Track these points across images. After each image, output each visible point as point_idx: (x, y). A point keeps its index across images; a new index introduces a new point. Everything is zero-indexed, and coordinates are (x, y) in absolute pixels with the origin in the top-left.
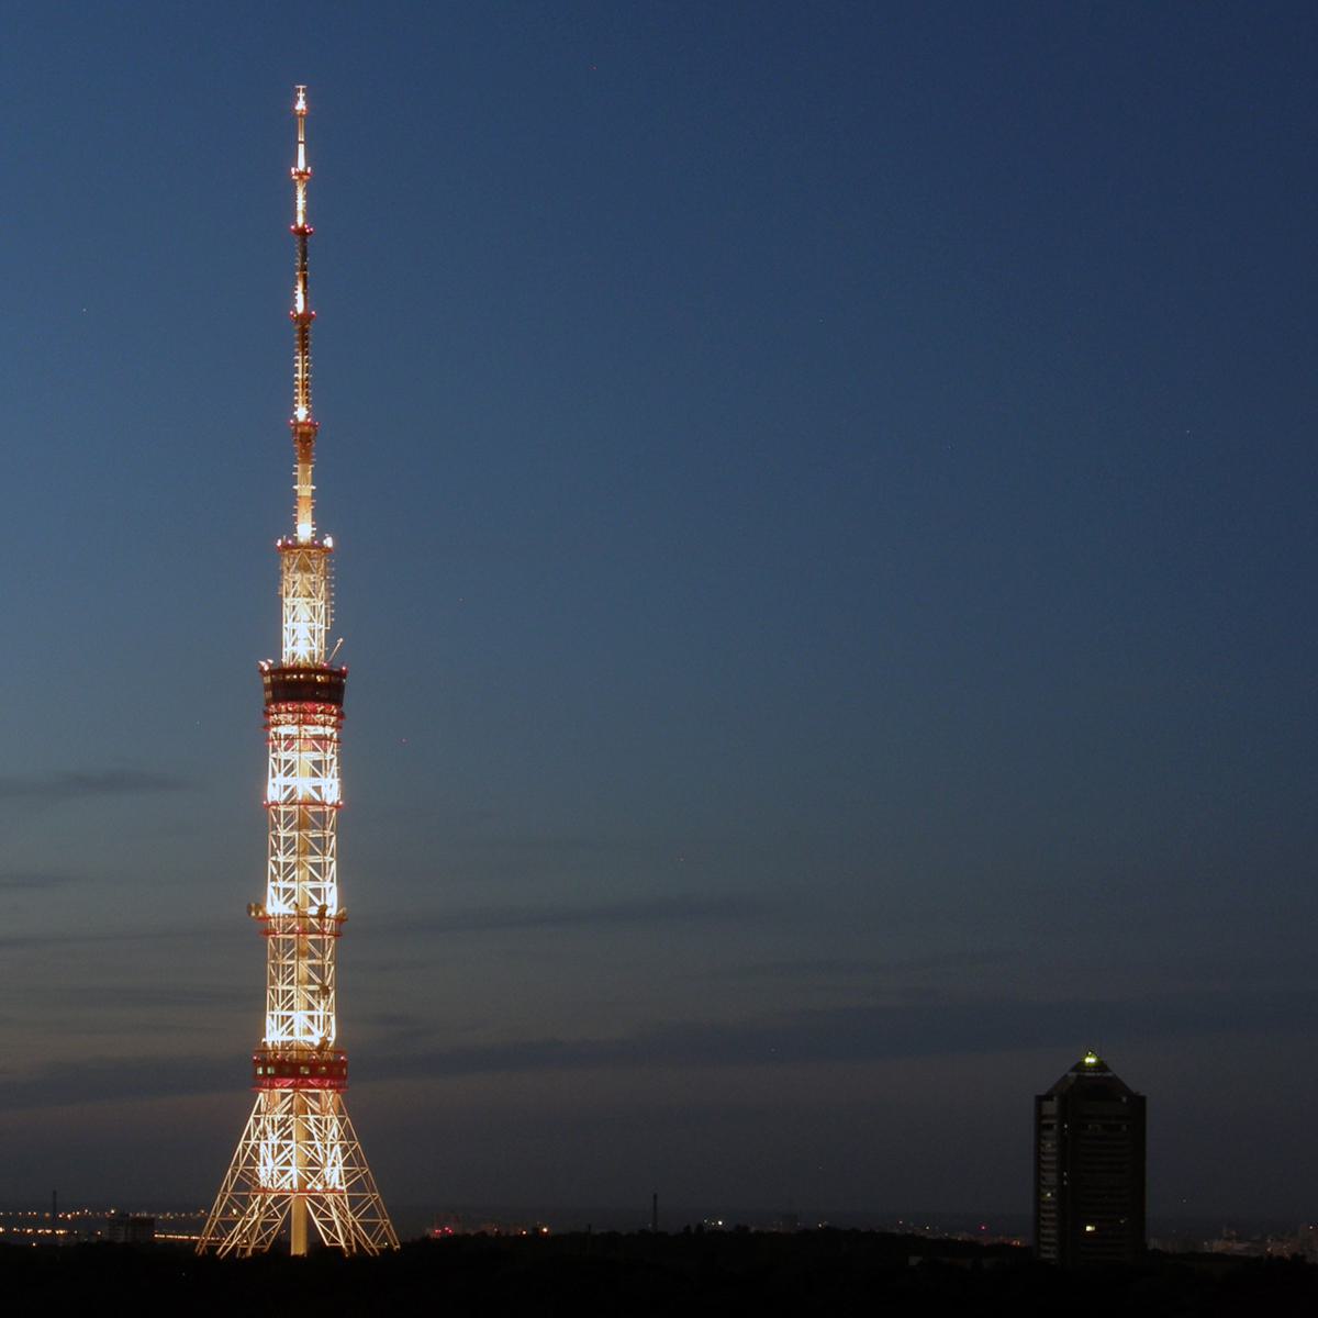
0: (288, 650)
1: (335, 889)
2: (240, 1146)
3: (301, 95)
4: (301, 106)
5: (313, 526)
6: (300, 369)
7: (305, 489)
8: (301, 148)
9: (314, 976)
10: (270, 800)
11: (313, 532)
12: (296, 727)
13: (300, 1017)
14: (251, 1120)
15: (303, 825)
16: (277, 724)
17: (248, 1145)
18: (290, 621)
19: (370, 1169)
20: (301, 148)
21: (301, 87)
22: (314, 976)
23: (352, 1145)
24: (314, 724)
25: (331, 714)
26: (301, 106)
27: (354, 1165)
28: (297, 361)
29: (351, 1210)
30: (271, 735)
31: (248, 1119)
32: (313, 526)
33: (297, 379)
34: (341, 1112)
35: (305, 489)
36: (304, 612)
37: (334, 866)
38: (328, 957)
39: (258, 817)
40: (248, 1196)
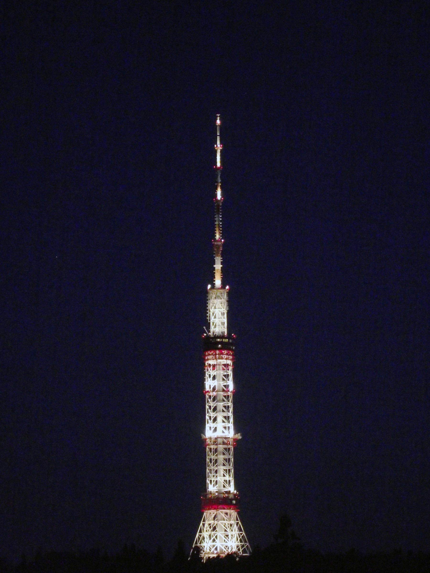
0: (212, 329)
1: (233, 481)
3: (218, 118)
4: (218, 122)
7: (218, 266)
8: (218, 138)
11: (221, 260)
14: (201, 524)
15: (224, 443)
16: (208, 360)
17: (200, 535)
19: (250, 544)
20: (218, 138)
21: (218, 115)
23: (241, 534)
24: (222, 358)
25: (230, 355)
26: (218, 122)
28: (216, 218)
30: (206, 364)
31: (200, 524)
32: (221, 260)
33: (216, 225)
35: (218, 266)
36: (218, 305)
37: (233, 459)
38: (231, 465)
40: (243, 554)
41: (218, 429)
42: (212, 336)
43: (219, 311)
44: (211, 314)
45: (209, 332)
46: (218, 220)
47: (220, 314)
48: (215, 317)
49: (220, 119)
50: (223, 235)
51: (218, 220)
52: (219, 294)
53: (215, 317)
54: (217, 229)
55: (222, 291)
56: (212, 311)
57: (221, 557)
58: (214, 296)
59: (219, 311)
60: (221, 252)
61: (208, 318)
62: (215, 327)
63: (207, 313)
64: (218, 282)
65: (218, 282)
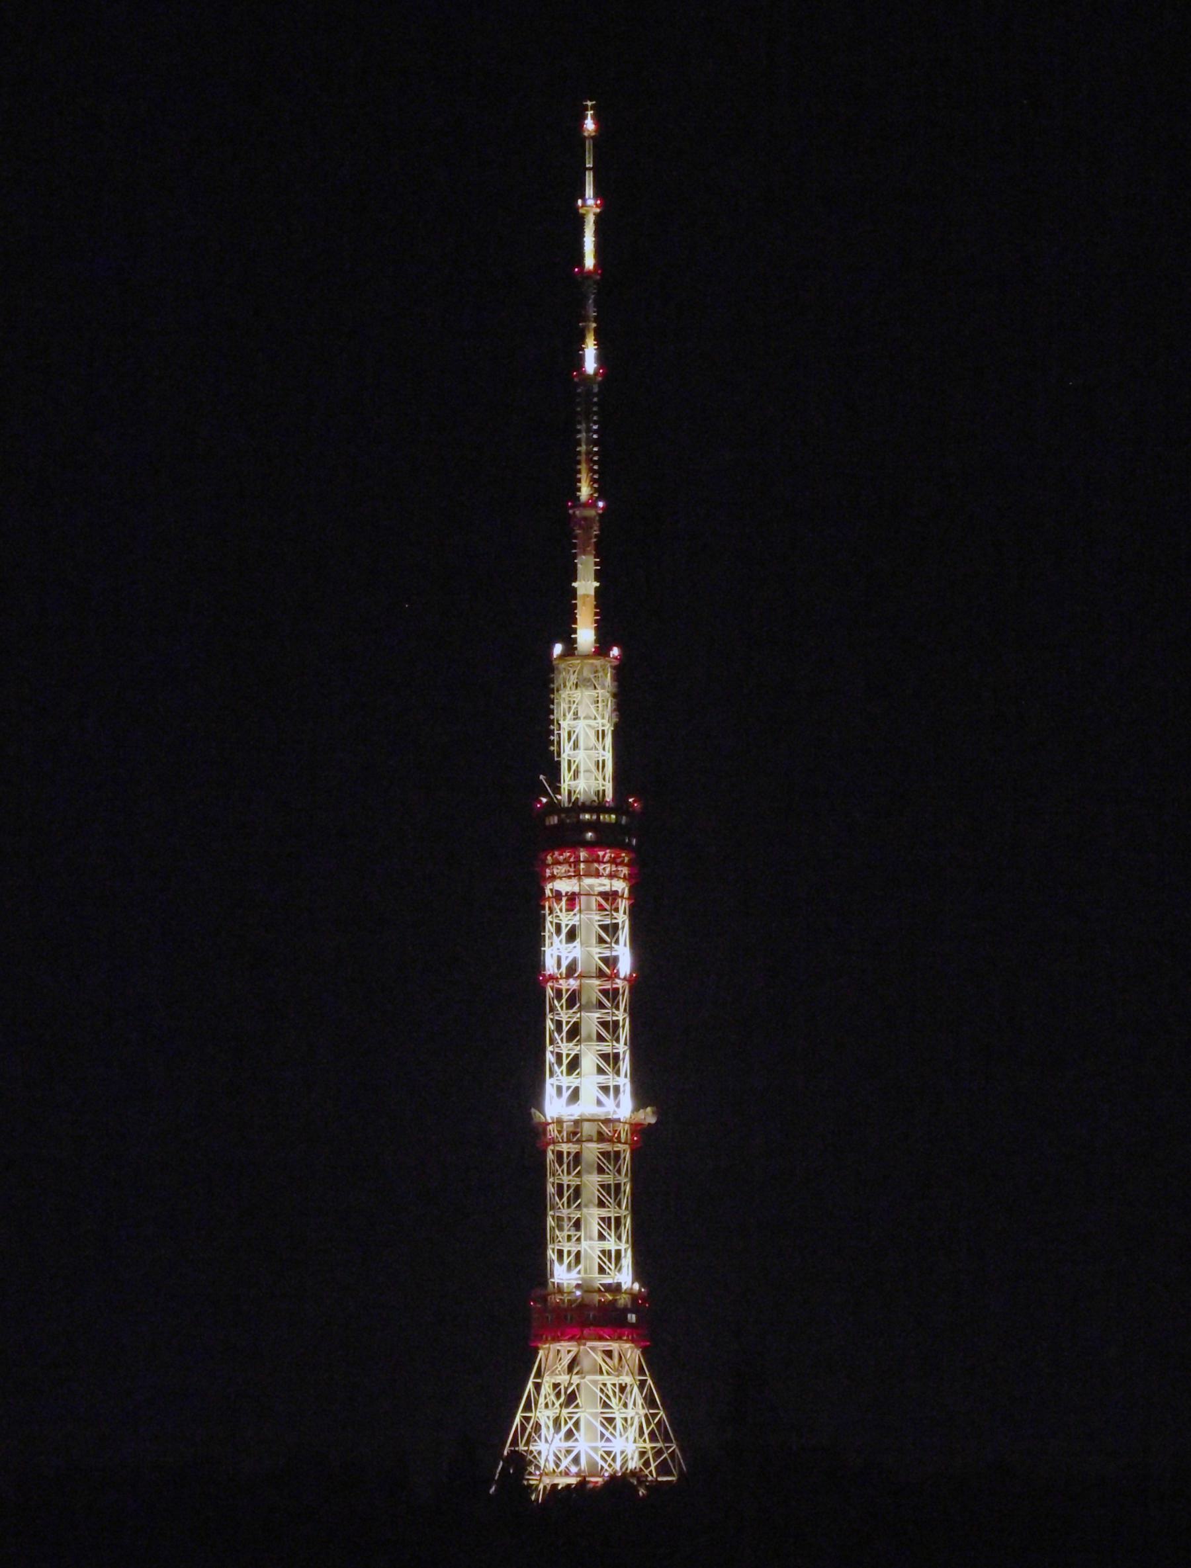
2: (517, 1420)
4: (590, 125)
5: (596, 564)
6: (584, 440)
7: (586, 586)
8: (589, 178)
9: (604, 1033)
10: (548, 973)
12: (574, 881)
13: (589, 1080)
17: (527, 1419)
18: (570, 716)
20: (589, 178)
21: (589, 103)
22: (604, 1033)
24: (598, 875)
25: (622, 863)
26: (590, 125)
27: (657, 1441)
28: (579, 432)
29: (655, 1461)
33: (579, 452)
34: (641, 1371)
35: (586, 586)
39: (527, 1141)
45: (557, 790)
46: (587, 439)
50: (602, 490)
51: (587, 439)
52: (587, 673)
54: (583, 467)
55: (598, 662)
58: (573, 678)
59: (589, 726)
62: (576, 775)
64: (586, 636)
65: (586, 636)
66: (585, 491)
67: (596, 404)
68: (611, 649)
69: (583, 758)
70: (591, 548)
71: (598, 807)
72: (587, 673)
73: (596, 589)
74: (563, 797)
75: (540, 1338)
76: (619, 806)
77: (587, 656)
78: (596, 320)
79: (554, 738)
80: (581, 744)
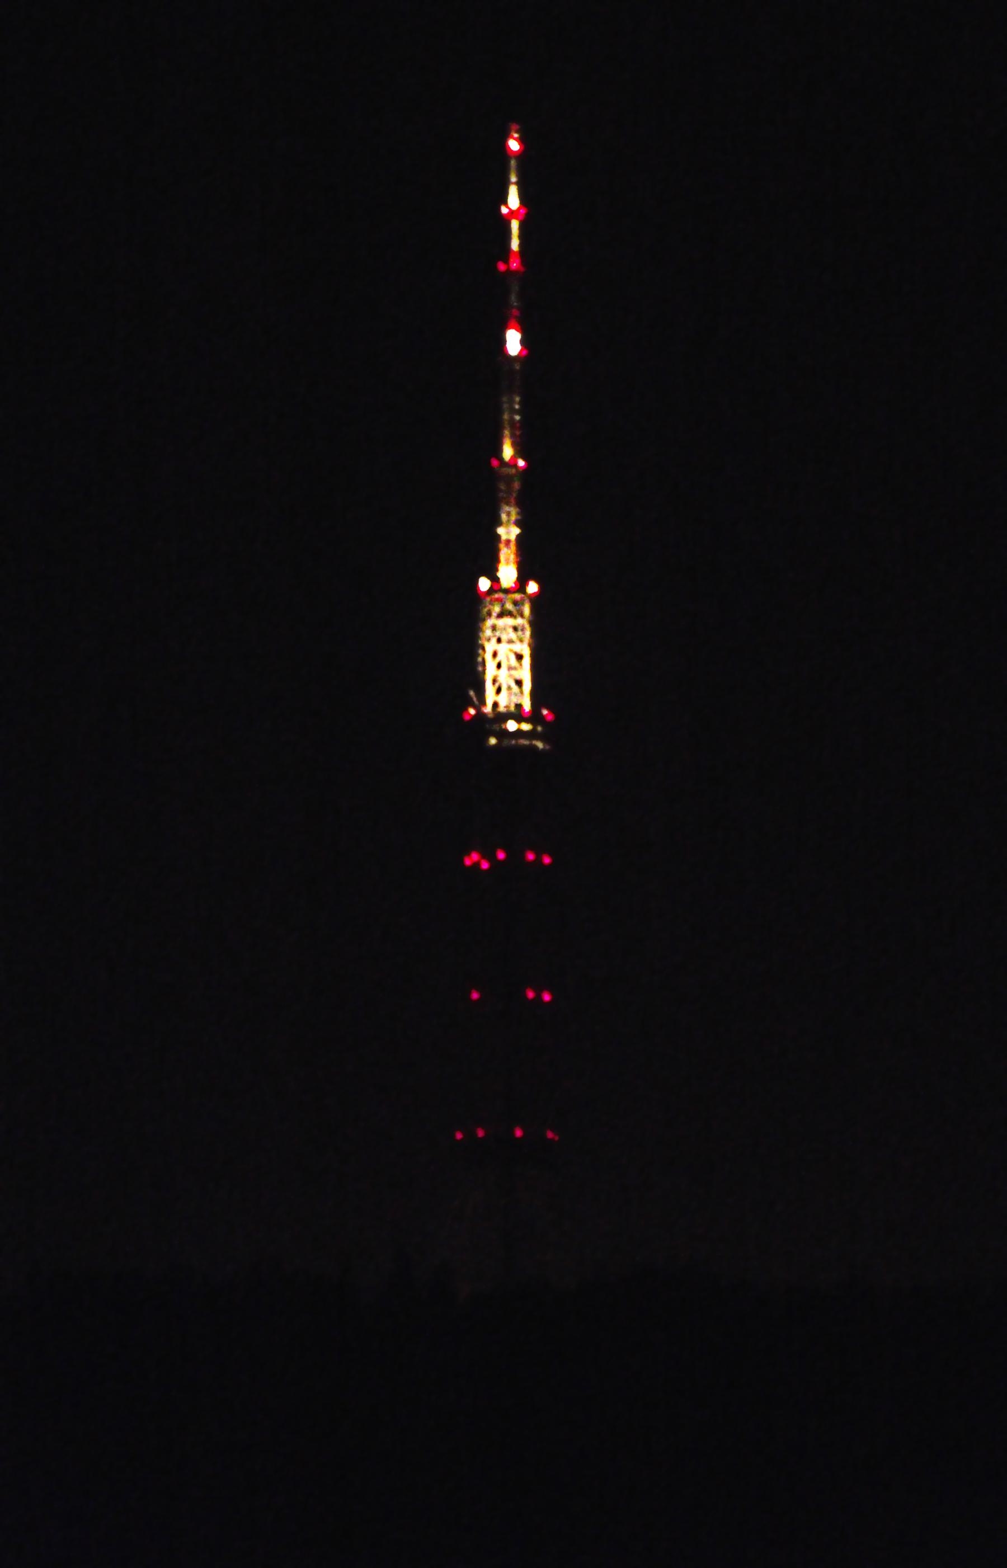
7: (509, 532)
18: (494, 640)
35: (509, 532)
41: (503, 665)
42: (491, 716)
43: (511, 650)
44: (488, 656)
45: (483, 702)
46: (513, 410)
47: (513, 657)
48: (499, 666)
49: (514, 445)
50: (520, 450)
51: (513, 410)
52: (509, 606)
53: (499, 691)
54: (507, 432)
55: (517, 596)
56: (490, 647)
57: (519, 517)
58: (497, 609)
59: (511, 650)
60: (515, 495)
61: (480, 669)
62: (499, 691)
63: (478, 655)
64: (508, 573)
65: (508, 573)
66: (508, 452)
67: (539, 996)
68: (524, 459)
69: (505, 678)
70: (513, 501)
71: (518, 715)
72: (509, 606)
73: (518, 537)
74: (488, 709)
75: (525, 352)
76: (534, 717)
77: (507, 591)
78: (516, 183)
79: (480, 659)
80: (504, 665)
